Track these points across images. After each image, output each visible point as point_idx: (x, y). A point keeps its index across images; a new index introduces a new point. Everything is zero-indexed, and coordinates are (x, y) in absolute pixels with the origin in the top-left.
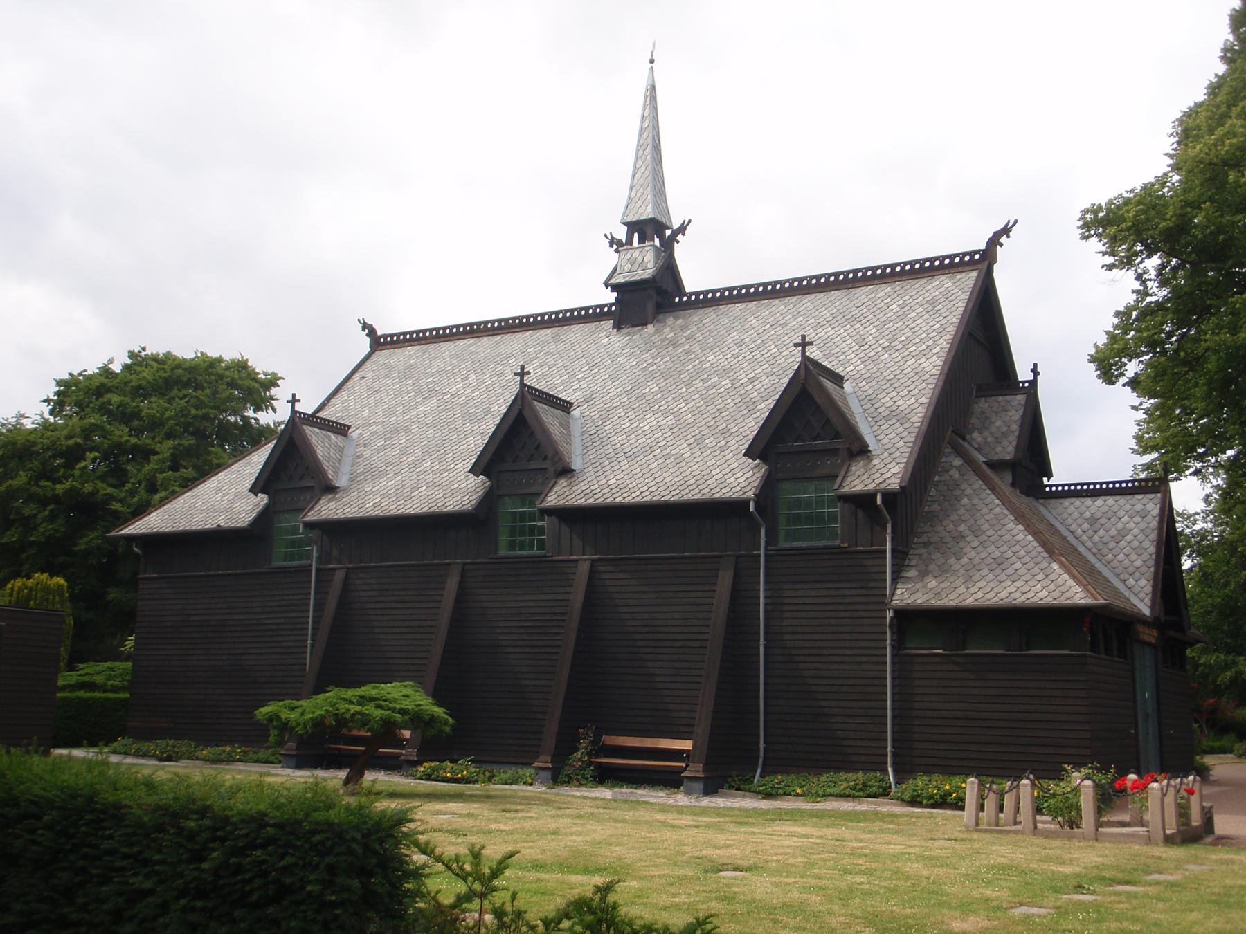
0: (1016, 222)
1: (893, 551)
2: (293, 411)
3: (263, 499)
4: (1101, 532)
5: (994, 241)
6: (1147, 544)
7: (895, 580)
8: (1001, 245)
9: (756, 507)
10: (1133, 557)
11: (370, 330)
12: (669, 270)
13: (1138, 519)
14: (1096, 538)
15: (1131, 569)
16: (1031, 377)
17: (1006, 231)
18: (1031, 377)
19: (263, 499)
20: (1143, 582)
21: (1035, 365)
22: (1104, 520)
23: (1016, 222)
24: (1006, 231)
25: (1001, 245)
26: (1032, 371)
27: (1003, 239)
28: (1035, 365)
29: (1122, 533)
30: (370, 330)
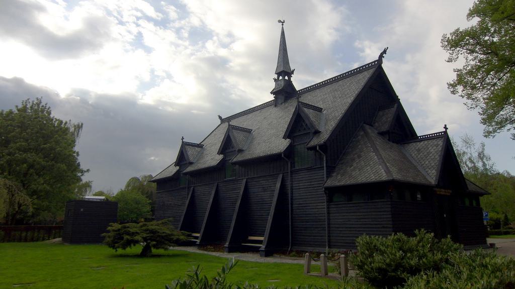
0: (387, 48)
1: (326, 166)
2: (183, 142)
3: (178, 168)
4: (421, 154)
5: (381, 56)
6: (437, 157)
7: (328, 177)
8: (384, 57)
9: (284, 156)
10: (432, 162)
11: (220, 117)
12: (289, 84)
13: (435, 147)
14: (419, 156)
15: (430, 167)
16: (444, 130)
17: (385, 52)
18: (444, 130)
19: (178, 168)
20: (434, 171)
21: (445, 125)
22: (422, 150)
23: (387, 48)
24: (385, 52)
25: (384, 57)
26: (444, 128)
27: (384, 55)
28: (445, 125)
29: (429, 153)
30: (220, 117)
